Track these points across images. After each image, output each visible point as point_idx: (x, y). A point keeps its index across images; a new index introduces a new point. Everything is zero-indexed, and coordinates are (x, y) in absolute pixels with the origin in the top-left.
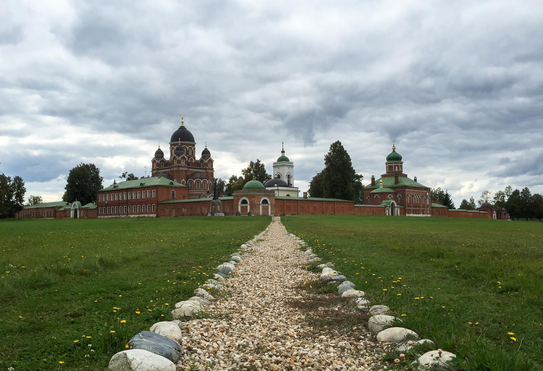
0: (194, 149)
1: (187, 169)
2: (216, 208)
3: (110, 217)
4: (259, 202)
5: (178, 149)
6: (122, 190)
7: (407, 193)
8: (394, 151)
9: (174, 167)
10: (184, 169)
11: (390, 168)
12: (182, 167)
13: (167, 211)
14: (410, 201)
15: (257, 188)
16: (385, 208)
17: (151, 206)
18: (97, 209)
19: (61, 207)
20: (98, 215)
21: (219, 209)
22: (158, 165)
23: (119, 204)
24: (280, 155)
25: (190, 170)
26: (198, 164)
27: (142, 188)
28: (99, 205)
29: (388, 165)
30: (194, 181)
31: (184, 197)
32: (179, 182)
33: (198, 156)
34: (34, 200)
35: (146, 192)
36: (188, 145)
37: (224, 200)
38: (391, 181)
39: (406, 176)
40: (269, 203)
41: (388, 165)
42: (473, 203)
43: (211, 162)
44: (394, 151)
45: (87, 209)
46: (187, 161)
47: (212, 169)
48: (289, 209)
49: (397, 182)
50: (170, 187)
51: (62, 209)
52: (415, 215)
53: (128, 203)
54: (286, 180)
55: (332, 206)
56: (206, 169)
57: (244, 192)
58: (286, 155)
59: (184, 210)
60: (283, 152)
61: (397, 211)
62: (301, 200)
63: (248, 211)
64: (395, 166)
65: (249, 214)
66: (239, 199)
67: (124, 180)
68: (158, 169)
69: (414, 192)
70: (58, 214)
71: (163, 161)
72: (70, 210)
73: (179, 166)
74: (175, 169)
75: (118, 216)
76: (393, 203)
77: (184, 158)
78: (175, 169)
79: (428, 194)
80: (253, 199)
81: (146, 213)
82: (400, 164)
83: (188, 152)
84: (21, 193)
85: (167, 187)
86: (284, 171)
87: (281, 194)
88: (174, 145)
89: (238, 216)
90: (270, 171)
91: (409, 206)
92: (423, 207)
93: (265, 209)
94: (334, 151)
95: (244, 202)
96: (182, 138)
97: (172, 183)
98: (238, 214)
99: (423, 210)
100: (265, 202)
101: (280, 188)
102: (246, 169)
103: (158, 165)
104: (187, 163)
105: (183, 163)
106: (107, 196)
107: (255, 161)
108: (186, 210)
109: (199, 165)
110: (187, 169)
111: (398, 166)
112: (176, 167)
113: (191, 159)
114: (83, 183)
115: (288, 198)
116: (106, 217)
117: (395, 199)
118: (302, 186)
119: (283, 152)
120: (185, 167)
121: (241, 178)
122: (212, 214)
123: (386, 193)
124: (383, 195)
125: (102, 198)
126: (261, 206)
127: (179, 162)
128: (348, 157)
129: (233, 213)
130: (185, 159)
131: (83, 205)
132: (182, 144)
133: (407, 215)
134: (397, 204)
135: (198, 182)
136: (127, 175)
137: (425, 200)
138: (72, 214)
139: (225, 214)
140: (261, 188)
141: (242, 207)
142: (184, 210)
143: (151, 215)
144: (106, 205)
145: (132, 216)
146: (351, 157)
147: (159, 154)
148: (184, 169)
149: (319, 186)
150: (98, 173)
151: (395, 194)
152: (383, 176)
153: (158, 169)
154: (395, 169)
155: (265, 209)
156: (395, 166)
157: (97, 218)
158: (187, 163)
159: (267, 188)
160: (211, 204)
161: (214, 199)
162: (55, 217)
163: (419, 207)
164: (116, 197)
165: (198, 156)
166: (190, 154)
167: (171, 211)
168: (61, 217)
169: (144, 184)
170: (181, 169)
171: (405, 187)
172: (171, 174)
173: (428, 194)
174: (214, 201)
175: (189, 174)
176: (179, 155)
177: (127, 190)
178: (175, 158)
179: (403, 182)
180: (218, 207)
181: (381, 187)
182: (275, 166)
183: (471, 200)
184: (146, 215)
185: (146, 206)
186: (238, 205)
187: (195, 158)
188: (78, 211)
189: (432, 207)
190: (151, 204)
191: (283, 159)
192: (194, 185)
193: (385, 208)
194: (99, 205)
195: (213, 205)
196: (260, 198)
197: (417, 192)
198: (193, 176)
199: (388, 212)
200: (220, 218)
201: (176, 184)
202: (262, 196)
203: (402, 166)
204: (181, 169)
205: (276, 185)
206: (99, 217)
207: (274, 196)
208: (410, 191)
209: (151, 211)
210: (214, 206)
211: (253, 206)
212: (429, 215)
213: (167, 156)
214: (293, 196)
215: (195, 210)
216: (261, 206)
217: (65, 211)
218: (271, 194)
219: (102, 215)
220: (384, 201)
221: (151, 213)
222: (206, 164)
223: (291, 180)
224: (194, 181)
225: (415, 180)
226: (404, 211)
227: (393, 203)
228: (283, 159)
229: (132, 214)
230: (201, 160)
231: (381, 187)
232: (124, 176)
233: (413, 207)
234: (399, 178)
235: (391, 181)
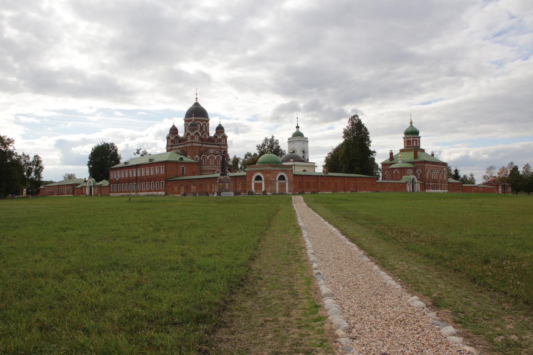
0: (208, 125)
1: (200, 145)
2: (224, 186)
3: (121, 194)
4: (275, 178)
5: (192, 125)
6: (132, 167)
7: (427, 168)
8: (411, 125)
9: (187, 143)
10: (197, 145)
11: (407, 142)
12: (195, 143)
13: (176, 188)
14: (429, 177)
15: (273, 162)
16: (406, 183)
17: (160, 183)
18: (109, 186)
19: (78, 184)
20: (110, 192)
21: (227, 188)
22: (173, 141)
23: (129, 180)
24: (295, 130)
25: (204, 145)
26: (211, 140)
27: (152, 164)
28: (112, 182)
29: (406, 140)
30: (208, 157)
31: (194, 174)
32: (193, 158)
33: (212, 133)
34: (69, 177)
35: (155, 168)
36: (202, 121)
37: (236, 177)
38: (410, 156)
39: (423, 151)
40: (287, 179)
41: (406, 140)
42: (472, 178)
43: (225, 137)
44: (411, 125)
45: (100, 187)
46: (201, 138)
47: (226, 145)
48: (307, 184)
49: (416, 156)
50: (180, 163)
51: (79, 186)
52: (434, 191)
53: (137, 180)
54: (301, 155)
55: (355, 182)
56: (219, 145)
57: (258, 167)
58: (301, 130)
59: (193, 188)
60: (298, 127)
61: (418, 187)
62: (321, 176)
63: (263, 189)
64: (413, 141)
65: (265, 193)
66: (252, 175)
67: (138, 156)
68: (172, 146)
69: (432, 167)
70: (76, 192)
71: (177, 137)
72: (85, 187)
73: (192, 142)
74: (189, 145)
75: (128, 194)
76: (413, 179)
77: (197, 134)
78: (189, 145)
79: (445, 169)
80: (268, 175)
81: (155, 191)
82: (417, 139)
83: (201, 128)
84: (39, 170)
85: (177, 162)
86: (298, 147)
87: (298, 170)
88: (188, 121)
89: (251, 197)
90: (284, 147)
91: (428, 182)
92: (441, 183)
93: (282, 186)
94: (353, 124)
95: (258, 178)
96: (197, 115)
97: (181, 159)
98: (251, 193)
99: (441, 185)
100: (282, 178)
101: (296, 163)
102: (261, 144)
103: (173, 141)
104: (201, 139)
105: (197, 139)
106: (118, 173)
107: (270, 137)
108: (195, 187)
109: (214, 141)
110: (200, 145)
111: (416, 141)
112: (189, 143)
113: (205, 136)
114: (103, 159)
115: (304, 173)
116: (117, 194)
117: (415, 174)
118: (318, 161)
119: (298, 127)
120: (199, 143)
121: (255, 154)
122: (219, 194)
123: (405, 168)
124: (403, 171)
125: (115, 175)
126: (277, 184)
127: (192, 138)
128: (366, 129)
129: (245, 191)
130: (199, 135)
131: (98, 180)
132: (196, 120)
133: (427, 191)
134: (418, 180)
135: (212, 158)
136: (141, 152)
137: (443, 175)
138: (87, 191)
139: (236, 193)
140: (278, 162)
141: (256, 184)
142: (193, 188)
143: (160, 193)
144: (118, 182)
145: (141, 194)
146: (369, 130)
147: (174, 130)
148: (197, 145)
149: (334, 161)
150: (116, 150)
151: (415, 169)
152: (401, 151)
153: (172, 146)
154: (413, 144)
155: (282, 186)
156: (413, 141)
157: (109, 195)
158: (201, 139)
159: (284, 164)
160: (217, 182)
161: (221, 175)
162: (73, 193)
163: (437, 182)
164: (133, 174)
165: (212, 133)
166: (204, 129)
167: (179, 188)
168: (78, 194)
169: (153, 159)
170: (194, 144)
171: (425, 162)
172: (185, 150)
173: (445, 169)
174: (222, 177)
175: (203, 150)
176: (193, 130)
177: (137, 166)
178: (188, 134)
179: (421, 157)
180: (227, 184)
181: (400, 162)
182: (290, 141)
183: (471, 176)
184: (155, 193)
185: (155, 183)
186: (251, 181)
187: (208, 134)
188: (93, 188)
189: (449, 183)
190: (160, 181)
191: (298, 135)
192: (208, 161)
193: (406, 183)
194: (112, 182)
195: (220, 182)
196: (277, 174)
197: (436, 167)
198: (206, 151)
199: (409, 188)
200: (229, 201)
201: (186, 159)
202: (279, 171)
203: (419, 141)
204: (194, 144)
205: (292, 160)
206: (111, 194)
207: (292, 171)
208: (429, 166)
209: (160, 189)
210: (221, 184)
211: (268, 183)
212: (446, 191)
213: (181, 134)
214: (309, 172)
215: (203, 188)
216: (277, 184)
217: (81, 188)
218: (289, 169)
219: (114, 192)
220: (404, 177)
221: (160, 191)
222: (220, 140)
223: (306, 155)
224: (208, 157)
225: (433, 155)
226: (424, 187)
227: (413, 179)
228: (298, 135)
229: (141, 191)
230: (215, 136)
231: (400, 162)
232: (138, 153)
233: (432, 182)
234: (418, 153)
235: (410, 156)
